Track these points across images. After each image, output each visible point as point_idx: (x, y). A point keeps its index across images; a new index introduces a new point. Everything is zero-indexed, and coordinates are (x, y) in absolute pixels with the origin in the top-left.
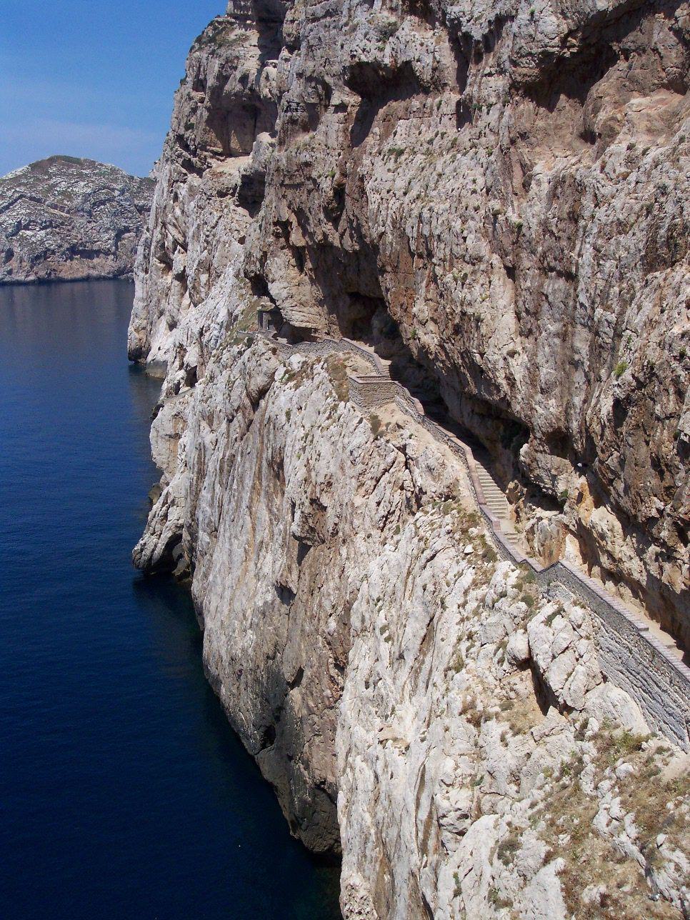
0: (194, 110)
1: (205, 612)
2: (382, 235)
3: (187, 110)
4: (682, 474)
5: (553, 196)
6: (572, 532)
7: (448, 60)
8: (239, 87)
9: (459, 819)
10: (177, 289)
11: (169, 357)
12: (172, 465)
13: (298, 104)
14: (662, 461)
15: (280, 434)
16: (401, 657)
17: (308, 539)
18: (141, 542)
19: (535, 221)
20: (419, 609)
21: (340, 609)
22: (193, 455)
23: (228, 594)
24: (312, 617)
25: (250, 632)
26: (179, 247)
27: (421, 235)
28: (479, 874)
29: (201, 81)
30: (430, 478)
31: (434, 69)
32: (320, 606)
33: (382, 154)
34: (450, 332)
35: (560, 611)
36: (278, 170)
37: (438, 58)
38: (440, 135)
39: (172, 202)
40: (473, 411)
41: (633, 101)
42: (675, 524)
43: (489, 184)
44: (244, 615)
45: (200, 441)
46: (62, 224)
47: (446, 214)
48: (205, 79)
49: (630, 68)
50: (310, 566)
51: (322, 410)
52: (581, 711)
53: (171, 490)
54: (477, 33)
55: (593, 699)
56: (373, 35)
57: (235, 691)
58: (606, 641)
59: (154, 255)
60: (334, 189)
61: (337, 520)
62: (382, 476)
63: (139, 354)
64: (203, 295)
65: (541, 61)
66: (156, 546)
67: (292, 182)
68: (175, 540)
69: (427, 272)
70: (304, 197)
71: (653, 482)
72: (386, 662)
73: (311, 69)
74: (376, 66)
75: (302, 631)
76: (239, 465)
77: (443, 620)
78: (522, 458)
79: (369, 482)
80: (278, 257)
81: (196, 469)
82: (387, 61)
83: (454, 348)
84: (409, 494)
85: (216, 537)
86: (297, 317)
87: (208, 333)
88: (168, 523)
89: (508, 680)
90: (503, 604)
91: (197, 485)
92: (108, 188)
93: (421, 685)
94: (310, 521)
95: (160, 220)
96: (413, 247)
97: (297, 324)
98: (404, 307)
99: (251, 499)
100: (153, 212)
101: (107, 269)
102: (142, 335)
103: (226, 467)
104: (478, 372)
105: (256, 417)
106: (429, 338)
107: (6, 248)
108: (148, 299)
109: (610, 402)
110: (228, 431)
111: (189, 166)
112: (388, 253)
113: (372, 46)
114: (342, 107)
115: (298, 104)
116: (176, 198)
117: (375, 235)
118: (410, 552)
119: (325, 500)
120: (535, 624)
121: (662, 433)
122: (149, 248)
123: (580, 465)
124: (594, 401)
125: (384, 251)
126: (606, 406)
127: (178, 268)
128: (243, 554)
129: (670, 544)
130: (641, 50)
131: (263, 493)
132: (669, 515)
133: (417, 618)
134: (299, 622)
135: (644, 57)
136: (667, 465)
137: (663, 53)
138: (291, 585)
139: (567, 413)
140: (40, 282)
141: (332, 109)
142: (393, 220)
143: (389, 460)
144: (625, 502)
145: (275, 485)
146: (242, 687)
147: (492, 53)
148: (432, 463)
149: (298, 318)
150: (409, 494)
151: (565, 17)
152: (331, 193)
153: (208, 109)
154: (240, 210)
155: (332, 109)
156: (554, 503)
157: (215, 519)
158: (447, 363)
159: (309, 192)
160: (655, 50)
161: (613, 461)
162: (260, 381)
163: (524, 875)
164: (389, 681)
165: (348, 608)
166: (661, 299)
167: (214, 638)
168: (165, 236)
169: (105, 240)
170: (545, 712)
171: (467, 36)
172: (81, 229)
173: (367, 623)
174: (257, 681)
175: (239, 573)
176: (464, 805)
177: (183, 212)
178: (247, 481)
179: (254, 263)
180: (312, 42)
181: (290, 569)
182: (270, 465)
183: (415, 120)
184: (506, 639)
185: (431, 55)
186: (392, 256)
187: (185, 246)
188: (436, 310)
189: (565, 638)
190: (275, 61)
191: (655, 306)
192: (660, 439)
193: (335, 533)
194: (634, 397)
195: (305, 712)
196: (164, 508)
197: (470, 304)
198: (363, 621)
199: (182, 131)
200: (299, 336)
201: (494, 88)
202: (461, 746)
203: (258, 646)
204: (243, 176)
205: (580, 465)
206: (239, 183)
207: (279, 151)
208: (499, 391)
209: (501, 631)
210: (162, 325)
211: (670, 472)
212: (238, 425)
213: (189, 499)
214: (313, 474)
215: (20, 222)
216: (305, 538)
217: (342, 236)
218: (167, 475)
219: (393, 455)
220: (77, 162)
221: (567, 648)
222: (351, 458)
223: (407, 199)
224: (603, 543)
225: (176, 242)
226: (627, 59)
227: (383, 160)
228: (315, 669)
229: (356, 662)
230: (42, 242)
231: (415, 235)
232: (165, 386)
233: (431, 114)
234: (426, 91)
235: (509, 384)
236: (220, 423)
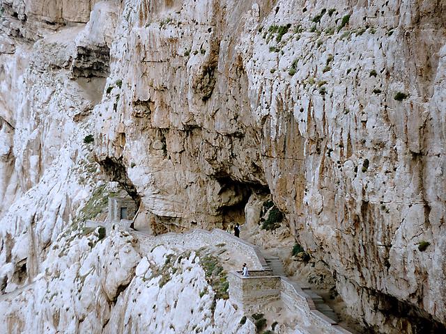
2: (265, 119)
38: (327, 12)
43: (389, 65)
51: (196, 309)
62: (118, 294)
64: (33, 179)
80: (139, 140)
111: (17, 34)
112: (273, 137)
125: (269, 134)
142: (279, 103)
162: (117, 276)
186: (278, 140)
207: (141, 25)
212: (89, 326)
223: (293, 80)
227: (264, 38)
231: (305, 118)
236: (67, 323)
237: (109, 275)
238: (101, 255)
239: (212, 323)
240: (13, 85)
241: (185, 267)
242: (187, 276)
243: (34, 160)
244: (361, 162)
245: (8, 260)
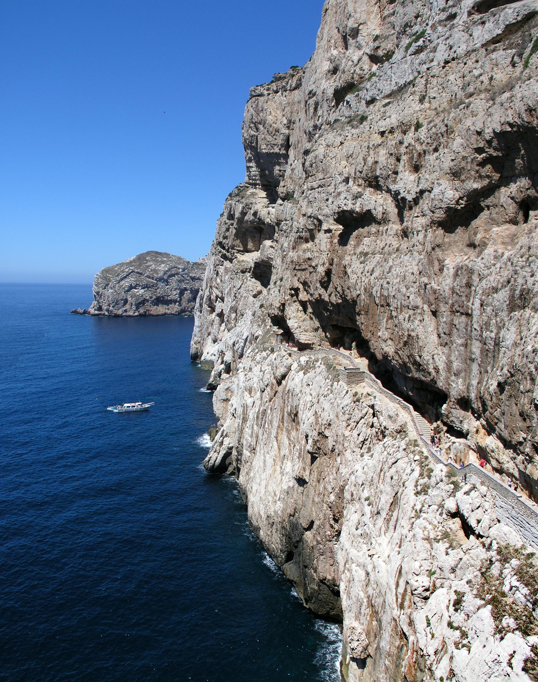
0: (228, 230)
1: (248, 493)
2: (358, 296)
3: (224, 229)
4: (535, 420)
5: (456, 275)
6: (473, 450)
7: (393, 210)
8: (252, 218)
9: (423, 591)
10: (218, 321)
11: (213, 358)
12: (224, 416)
13: (303, 229)
14: (525, 413)
15: (295, 399)
16: (378, 513)
17: (317, 453)
18: (209, 456)
19: (447, 287)
20: (388, 489)
21: (337, 489)
22: (240, 410)
23: (264, 483)
24: (319, 494)
25: (278, 502)
26: (219, 299)
27: (382, 295)
28: (440, 616)
29: (232, 215)
30: (390, 422)
31: (383, 213)
32: (325, 488)
34: (401, 345)
35: (474, 488)
36: (292, 262)
37: (385, 208)
39: (215, 276)
40: (413, 387)
41: (494, 229)
42: (533, 445)
44: (275, 494)
45: (244, 402)
46: (153, 286)
47: (397, 285)
48: (234, 214)
49: (491, 214)
50: (318, 468)
52: (487, 538)
53: (225, 429)
54: (409, 198)
55: (493, 532)
56: (350, 197)
57: (269, 533)
58: (499, 503)
59: (205, 303)
60: (325, 271)
61: (334, 443)
63: (196, 357)
64: (233, 325)
65: (446, 211)
66: (217, 459)
67: (300, 268)
68: (228, 454)
69: (386, 314)
70: (308, 275)
71: (520, 424)
72: (368, 515)
73: (311, 212)
74: (351, 212)
77: (404, 494)
78: (443, 412)
79: (353, 424)
81: (241, 418)
82: (358, 209)
83: (403, 353)
84: (377, 430)
85: (254, 453)
86: (303, 338)
87: (238, 345)
88: (223, 446)
89: (445, 523)
90: (441, 485)
91: (242, 425)
92: (176, 267)
93: (391, 528)
94: (318, 444)
95: (209, 285)
96: (377, 302)
97: (303, 342)
98: (372, 332)
99: (277, 433)
100: (205, 281)
101: (175, 310)
102: (198, 346)
103: (260, 416)
104: (418, 366)
105: (280, 389)
106: (389, 349)
107: (124, 298)
108: (201, 326)
109: (496, 384)
110: (262, 397)
111: (225, 257)
112: (362, 305)
113: (350, 202)
114: (329, 231)
115: (303, 229)
116: (217, 274)
117: (355, 296)
118: (381, 460)
119: (327, 433)
120: (459, 495)
121: (524, 399)
122: (203, 299)
123: (476, 415)
124: (484, 383)
126: (493, 386)
127: (218, 310)
128: (273, 462)
129: (531, 455)
130: (495, 206)
131: (284, 430)
132: (530, 440)
133: (387, 494)
134: (311, 497)
135: (497, 209)
136: (527, 416)
137: (506, 207)
138: (305, 477)
139: (468, 389)
140: (141, 315)
141: (323, 232)
143: (364, 412)
144: (505, 434)
145: (292, 426)
146: (274, 531)
147: (418, 206)
148: (391, 413)
149: (303, 338)
150: (377, 430)
151: (457, 191)
152: (324, 274)
153: (236, 229)
154: (253, 280)
155: (323, 232)
156: (460, 434)
157: (253, 443)
158: (400, 361)
159: (311, 273)
160: (502, 206)
161: (497, 413)
162: (282, 371)
163: (467, 615)
164: (371, 526)
165: (342, 490)
166: (520, 332)
167: (255, 506)
168: (211, 293)
169: (174, 295)
170: (468, 538)
171: (404, 199)
172: (162, 290)
173: (355, 496)
174: (283, 528)
175: (271, 472)
176: (427, 584)
177: (221, 281)
178: (274, 423)
179: (274, 309)
180: (311, 200)
181: (304, 469)
182: (289, 414)
183: (374, 238)
184: (443, 503)
185: (381, 207)
187: (222, 299)
188: (393, 334)
189: (478, 501)
190: (273, 205)
191: (517, 335)
193: (333, 450)
194: (509, 381)
195: (315, 543)
196: (222, 438)
197: (413, 330)
198: (352, 495)
199: (221, 240)
200: (303, 347)
201: (420, 223)
202: (423, 556)
203: (284, 510)
204: (255, 263)
205: (476, 415)
206: (253, 266)
207: (293, 252)
208: (430, 375)
209: (440, 499)
210: (210, 340)
211: (529, 419)
213: (237, 433)
214: (320, 419)
215: (131, 285)
216: (315, 453)
217: (330, 295)
218: (221, 420)
219: (366, 410)
220: (160, 254)
221: (479, 507)
222: (343, 411)
224: (493, 454)
225: (217, 297)
226: (488, 209)
228: (321, 521)
229: (348, 517)
230: (142, 296)
231: (379, 295)
232: (213, 373)
233: (382, 235)
234: (379, 223)
235: (435, 372)
236: (256, 393)
237: (278, 370)
238: (273, 360)
239: (332, 392)
240: (223, 279)
241: (316, 366)
242: (318, 370)
243: (233, 315)
244: (407, 316)
245: (222, 363)
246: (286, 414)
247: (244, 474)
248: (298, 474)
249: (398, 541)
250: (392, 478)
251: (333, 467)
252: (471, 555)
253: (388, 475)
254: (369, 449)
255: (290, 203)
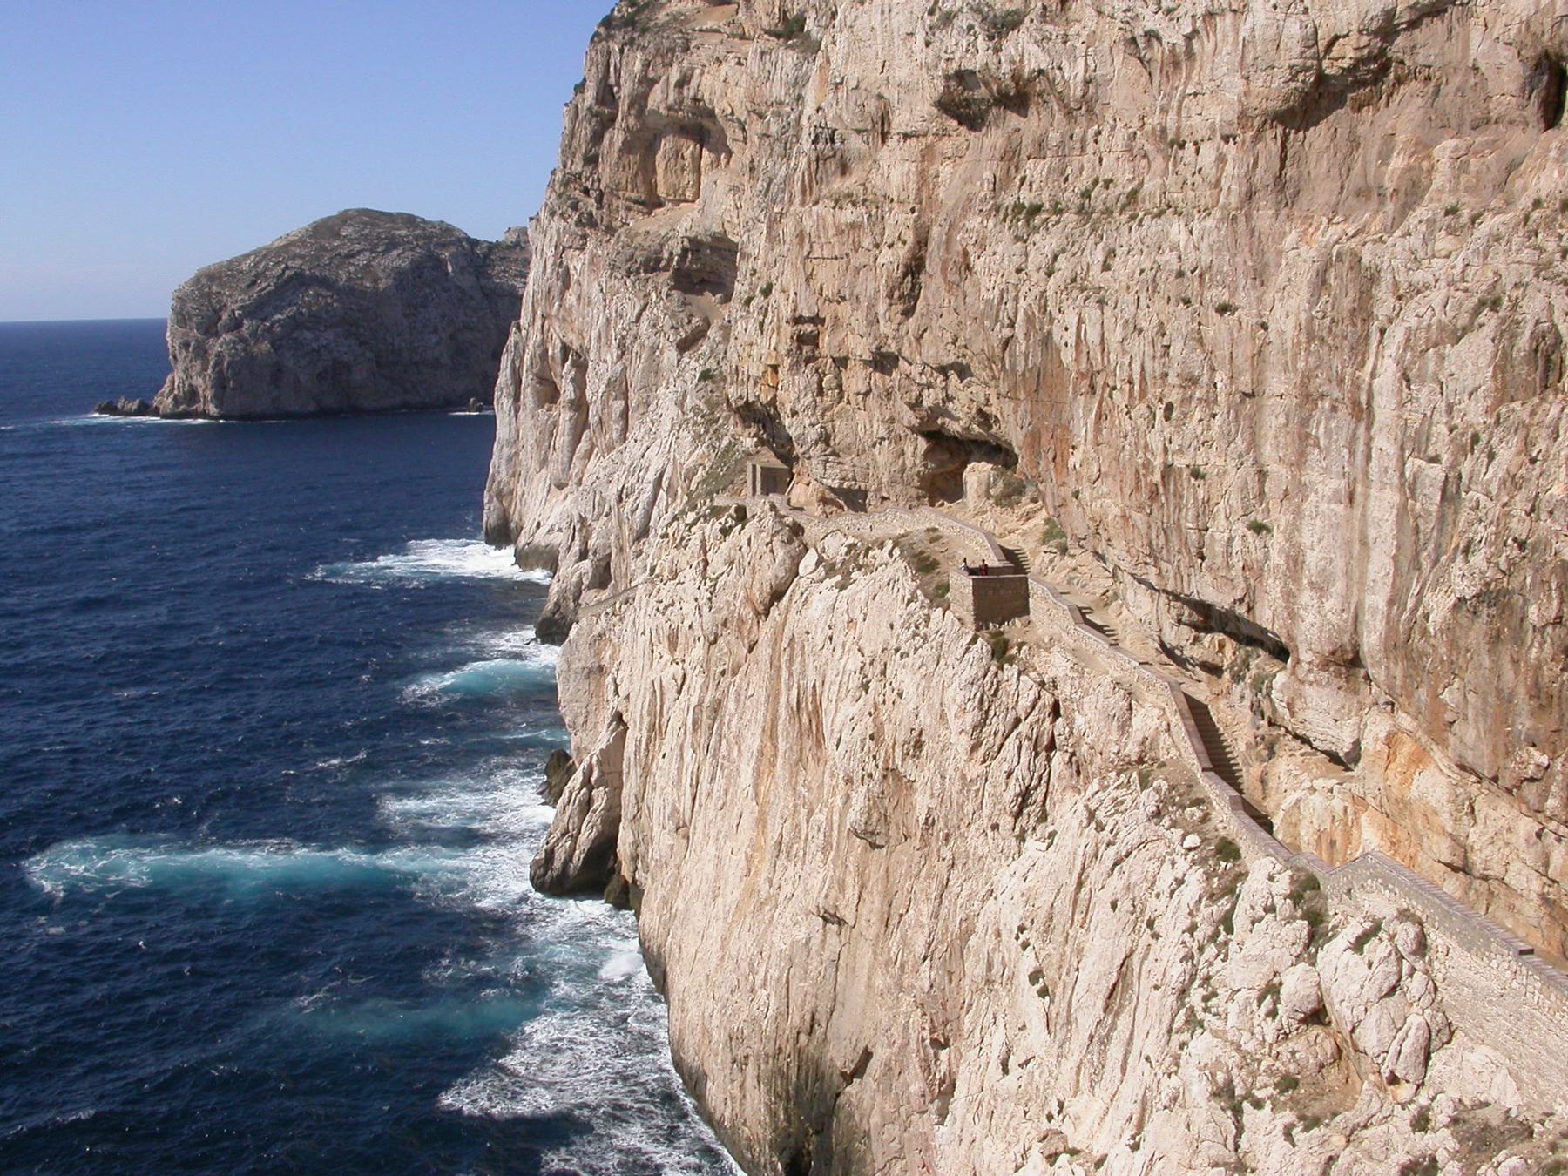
5: (1321, 283)
11: (559, 539)
19: (1291, 322)
31: (1087, 82)
33: (1002, 211)
38: (1101, 183)
75: (869, 986)
76: (732, 715)
103: (706, 721)
112: (1020, 369)
119: (909, 770)
192: (1537, 659)
233: (1083, 149)
245: (583, 555)
246: (783, 713)
247: (655, 905)
248: (821, 900)
249: (1136, 1109)
250: (1114, 906)
251: (928, 877)
252: (1366, 1144)
253: (1104, 897)
254: (1043, 817)
255: (792, 47)
